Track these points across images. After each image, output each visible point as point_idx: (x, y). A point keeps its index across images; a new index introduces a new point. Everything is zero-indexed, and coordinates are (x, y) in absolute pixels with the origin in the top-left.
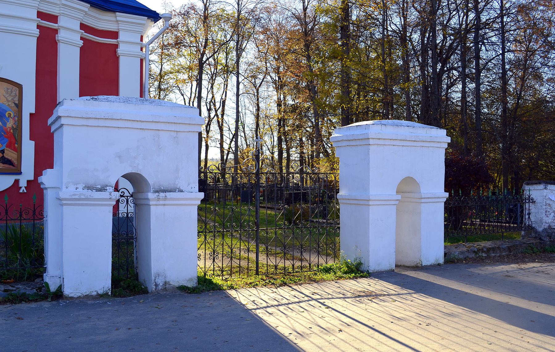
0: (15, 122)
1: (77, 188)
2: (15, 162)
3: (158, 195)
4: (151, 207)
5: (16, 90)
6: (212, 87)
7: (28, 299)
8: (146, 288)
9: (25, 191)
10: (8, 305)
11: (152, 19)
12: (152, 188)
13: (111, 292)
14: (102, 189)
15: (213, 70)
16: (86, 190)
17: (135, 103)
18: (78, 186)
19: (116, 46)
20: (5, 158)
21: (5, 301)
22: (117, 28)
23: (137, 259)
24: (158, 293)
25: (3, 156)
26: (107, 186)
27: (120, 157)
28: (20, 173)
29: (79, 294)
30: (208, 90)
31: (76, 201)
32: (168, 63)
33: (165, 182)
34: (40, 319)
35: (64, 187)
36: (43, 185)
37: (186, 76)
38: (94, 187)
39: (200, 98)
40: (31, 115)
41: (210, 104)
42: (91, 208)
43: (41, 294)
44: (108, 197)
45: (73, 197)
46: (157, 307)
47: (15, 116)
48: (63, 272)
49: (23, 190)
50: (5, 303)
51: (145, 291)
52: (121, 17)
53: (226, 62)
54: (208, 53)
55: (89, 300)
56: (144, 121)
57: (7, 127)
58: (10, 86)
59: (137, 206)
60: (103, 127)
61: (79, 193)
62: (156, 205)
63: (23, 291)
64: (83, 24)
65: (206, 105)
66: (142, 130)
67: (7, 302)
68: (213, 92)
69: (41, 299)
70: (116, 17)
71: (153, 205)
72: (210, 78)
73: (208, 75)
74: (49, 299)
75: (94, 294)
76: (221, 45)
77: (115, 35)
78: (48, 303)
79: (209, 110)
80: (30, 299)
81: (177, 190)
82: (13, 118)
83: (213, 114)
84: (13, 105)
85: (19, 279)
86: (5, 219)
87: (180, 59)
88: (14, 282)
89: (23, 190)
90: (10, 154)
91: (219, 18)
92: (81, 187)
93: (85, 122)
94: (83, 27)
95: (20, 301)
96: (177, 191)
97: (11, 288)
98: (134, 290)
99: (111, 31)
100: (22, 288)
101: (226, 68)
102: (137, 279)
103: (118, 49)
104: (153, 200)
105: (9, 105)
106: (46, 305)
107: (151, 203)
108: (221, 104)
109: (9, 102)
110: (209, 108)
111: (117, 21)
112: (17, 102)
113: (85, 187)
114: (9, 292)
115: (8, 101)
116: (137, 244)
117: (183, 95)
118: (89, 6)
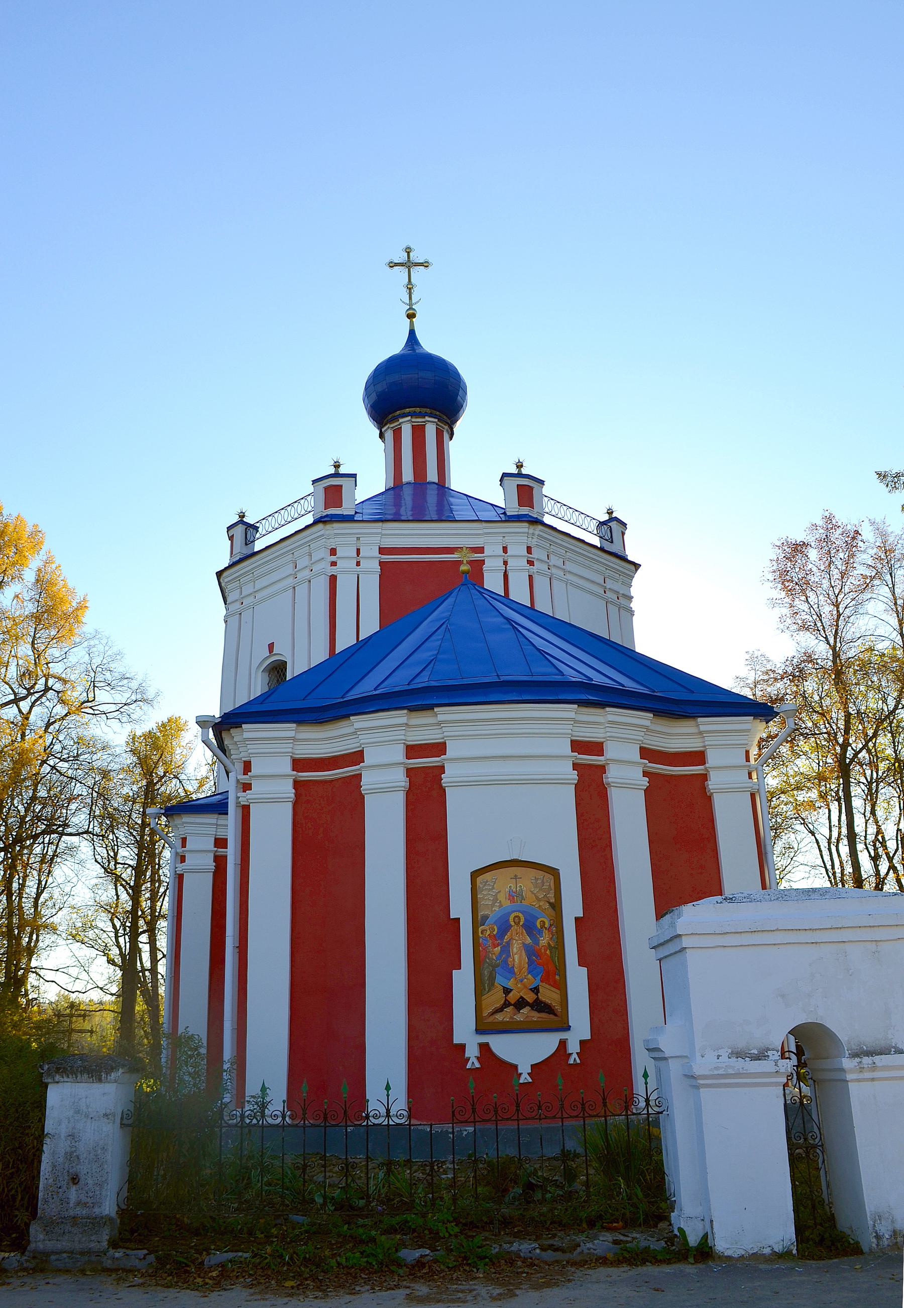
0: (553, 936)
1: (718, 1057)
2: (558, 1008)
3: (860, 1062)
4: (849, 1083)
5: (549, 878)
6: (873, 812)
7: (654, 1258)
8: (857, 1243)
9: (578, 1061)
10: (625, 1268)
11: (761, 718)
12: (846, 1048)
13: (797, 1250)
14: (760, 1056)
15: (868, 772)
16: (734, 1059)
17: (796, 898)
18: (720, 1052)
19: (704, 777)
20: (541, 1002)
21: (619, 1260)
22: (701, 745)
23: (828, 1186)
24: (884, 1254)
25: (538, 998)
26: (768, 1049)
27: (783, 996)
28: (568, 1028)
29: (740, 1250)
30: (865, 816)
31: (720, 1080)
32: (774, 773)
33: (870, 1036)
34: (692, 1292)
35: (698, 1055)
36: (660, 1053)
37: (814, 794)
38: (747, 1053)
39: (852, 837)
40: (577, 919)
41: (874, 846)
42: (746, 1090)
43: (674, 1250)
44: (773, 1069)
45: (716, 1072)
46: (893, 1279)
47: (551, 925)
48: (710, 1210)
49: (574, 1059)
50: (619, 1264)
51: (855, 1250)
52: (707, 724)
53: (895, 752)
54: (856, 744)
55: (761, 1263)
56: (816, 929)
57: (540, 946)
58: (540, 874)
59: (816, 1083)
60: (748, 945)
61: (724, 1065)
62: (858, 1080)
63: (643, 1244)
64: (645, 748)
65: (867, 848)
66: (814, 945)
67: (622, 1263)
68: (876, 822)
69: (676, 1258)
70: (698, 726)
71: (852, 1081)
72: (866, 792)
73: (862, 785)
74: (691, 1260)
75: (767, 1251)
76: (879, 722)
77: (699, 757)
78: (690, 1266)
79: (875, 859)
80: (659, 1257)
81: (893, 1050)
82: (549, 929)
83: (884, 867)
84: (547, 906)
85: (630, 1223)
86: (603, 1114)
87: (798, 762)
88: (624, 1227)
89: (574, 1059)
90: (548, 995)
91: (864, 667)
92: (725, 1053)
93: (720, 940)
94: (646, 753)
95: (644, 1262)
96: (892, 1053)
97: (622, 1238)
98: (833, 1248)
99: (691, 752)
100: (640, 1239)
101: (897, 764)
102: (834, 1226)
103: (709, 783)
104: (852, 1071)
105: (540, 906)
106: (689, 1269)
107: (849, 1077)
108: (899, 842)
109: (540, 901)
110: (873, 855)
111: (701, 733)
112: (552, 900)
113: (732, 1053)
114: (622, 1245)
115: (539, 900)
116: (825, 1156)
117: (813, 834)
118: (652, 715)
